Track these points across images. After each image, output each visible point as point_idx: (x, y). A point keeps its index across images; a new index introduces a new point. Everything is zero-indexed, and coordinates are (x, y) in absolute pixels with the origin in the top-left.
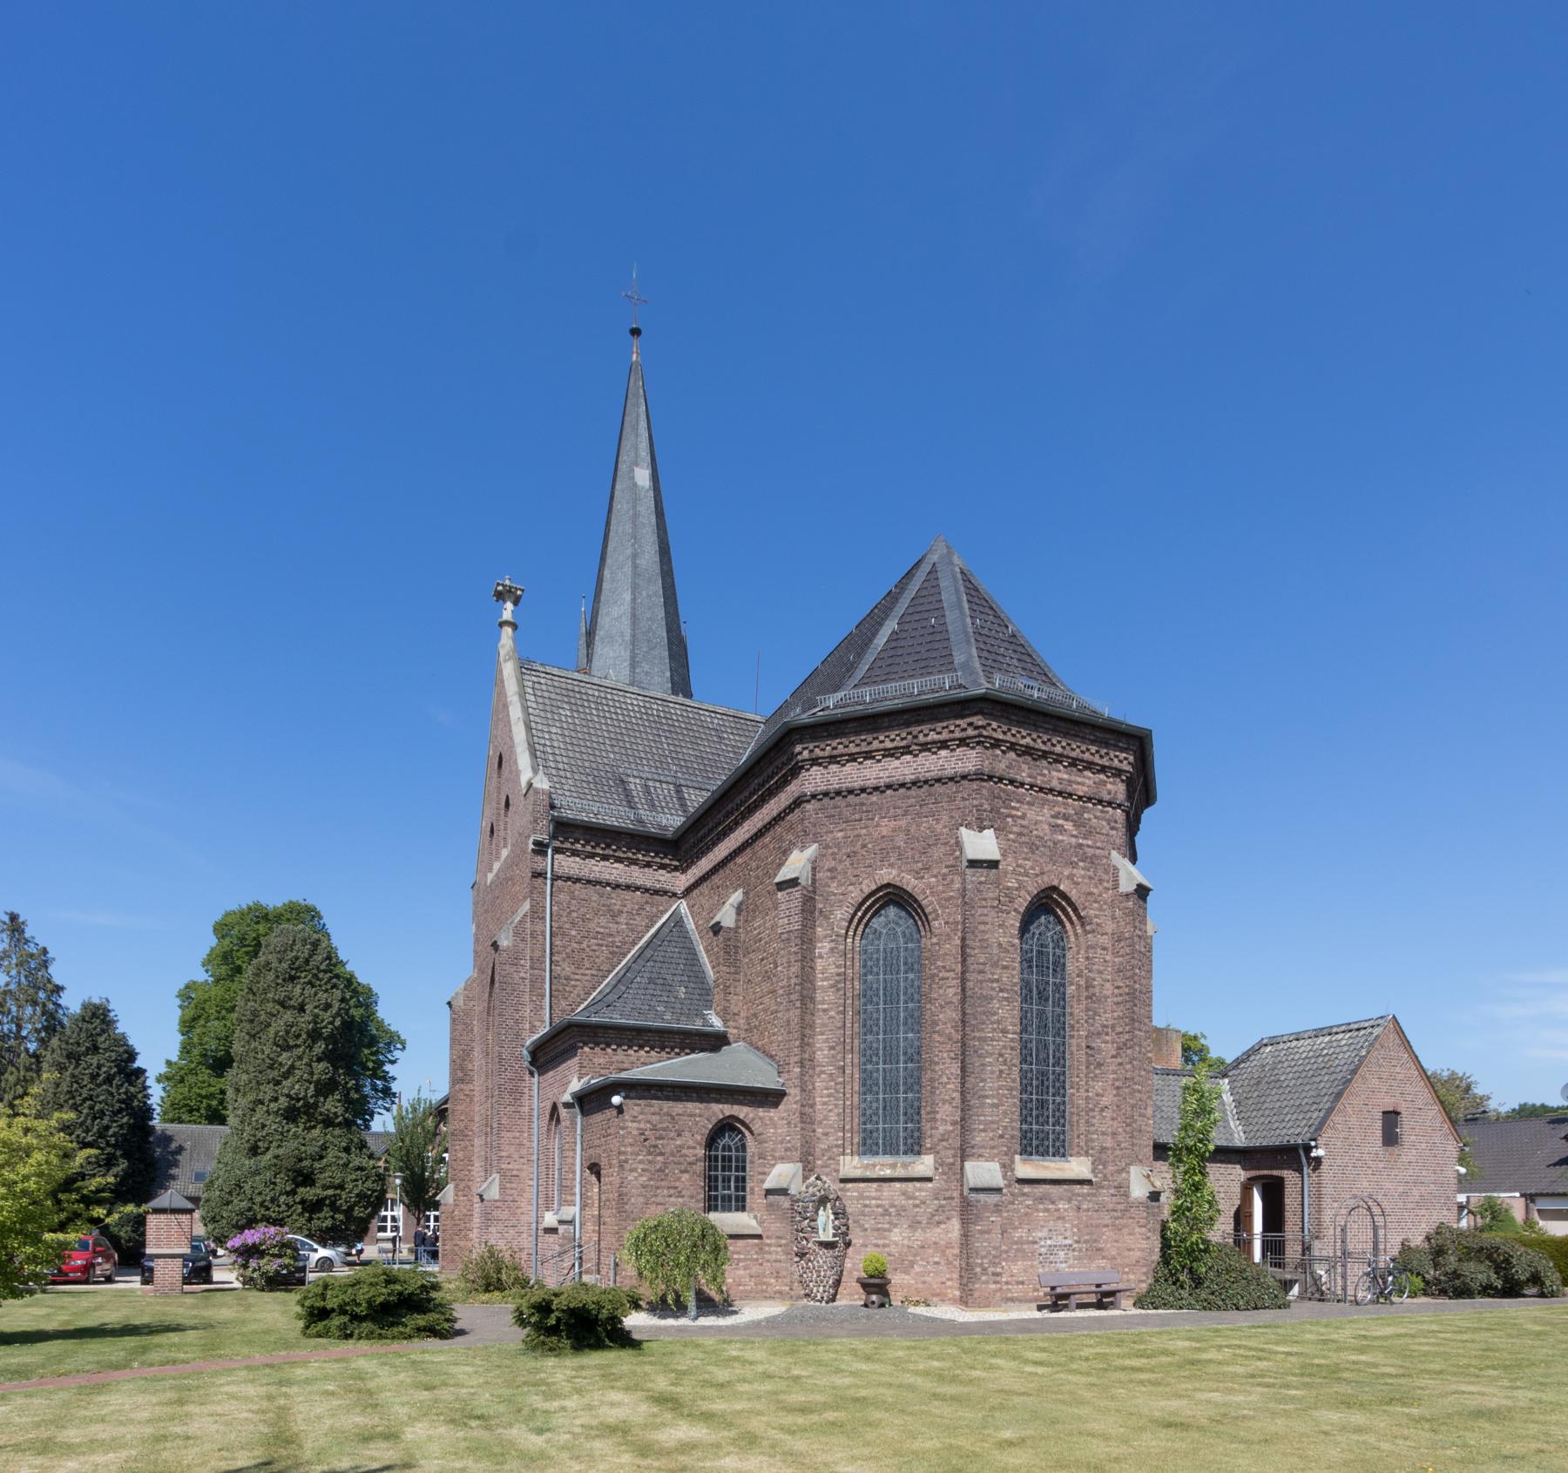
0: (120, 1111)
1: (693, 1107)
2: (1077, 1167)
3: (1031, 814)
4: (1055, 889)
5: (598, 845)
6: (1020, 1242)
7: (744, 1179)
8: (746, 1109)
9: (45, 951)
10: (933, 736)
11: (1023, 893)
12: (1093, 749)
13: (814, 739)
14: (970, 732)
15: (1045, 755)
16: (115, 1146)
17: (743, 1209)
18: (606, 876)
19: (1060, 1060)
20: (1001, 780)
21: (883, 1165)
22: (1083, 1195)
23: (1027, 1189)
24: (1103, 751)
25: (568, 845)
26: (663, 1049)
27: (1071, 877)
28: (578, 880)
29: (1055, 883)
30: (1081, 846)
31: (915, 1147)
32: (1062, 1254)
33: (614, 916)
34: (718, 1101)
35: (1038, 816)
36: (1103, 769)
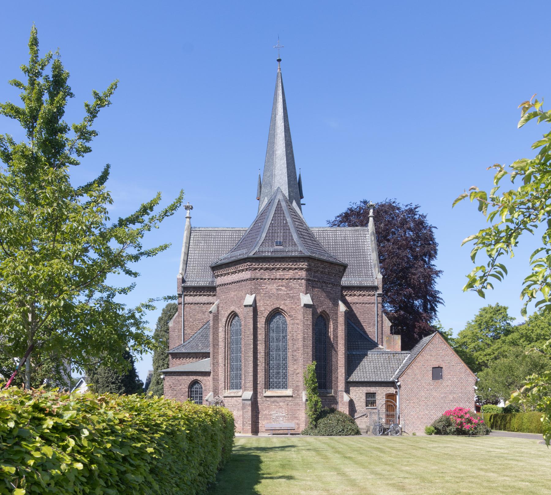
1: (184, 377)
2: (289, 392)
4: (279, 308)
5: (197, 292)
6: (266, 415)
7: (202, 397)
8: (200, 377)
10: (241, 268)
11: (266, 311)
12: (291, 264)
13: (217, 270)
14: (248, 267)
15: (273, 269)
16: (121, 383)
18: (201, 301)
19: (285, 359)
20: (258, 279)
21: (232, 392)
22: (289, 401)
23: (268, 399)
24: (295, 264)
25: (188, 293)
26: (197, 358)
27: (284, 304)
28: (192, 304)
29: (278, 306)
30: (288, 294)
31: (285, 387)
32: (281, 418)
33: (204, 313)
34: (192, 375)
35: (272, 287)
36: (296, 269)
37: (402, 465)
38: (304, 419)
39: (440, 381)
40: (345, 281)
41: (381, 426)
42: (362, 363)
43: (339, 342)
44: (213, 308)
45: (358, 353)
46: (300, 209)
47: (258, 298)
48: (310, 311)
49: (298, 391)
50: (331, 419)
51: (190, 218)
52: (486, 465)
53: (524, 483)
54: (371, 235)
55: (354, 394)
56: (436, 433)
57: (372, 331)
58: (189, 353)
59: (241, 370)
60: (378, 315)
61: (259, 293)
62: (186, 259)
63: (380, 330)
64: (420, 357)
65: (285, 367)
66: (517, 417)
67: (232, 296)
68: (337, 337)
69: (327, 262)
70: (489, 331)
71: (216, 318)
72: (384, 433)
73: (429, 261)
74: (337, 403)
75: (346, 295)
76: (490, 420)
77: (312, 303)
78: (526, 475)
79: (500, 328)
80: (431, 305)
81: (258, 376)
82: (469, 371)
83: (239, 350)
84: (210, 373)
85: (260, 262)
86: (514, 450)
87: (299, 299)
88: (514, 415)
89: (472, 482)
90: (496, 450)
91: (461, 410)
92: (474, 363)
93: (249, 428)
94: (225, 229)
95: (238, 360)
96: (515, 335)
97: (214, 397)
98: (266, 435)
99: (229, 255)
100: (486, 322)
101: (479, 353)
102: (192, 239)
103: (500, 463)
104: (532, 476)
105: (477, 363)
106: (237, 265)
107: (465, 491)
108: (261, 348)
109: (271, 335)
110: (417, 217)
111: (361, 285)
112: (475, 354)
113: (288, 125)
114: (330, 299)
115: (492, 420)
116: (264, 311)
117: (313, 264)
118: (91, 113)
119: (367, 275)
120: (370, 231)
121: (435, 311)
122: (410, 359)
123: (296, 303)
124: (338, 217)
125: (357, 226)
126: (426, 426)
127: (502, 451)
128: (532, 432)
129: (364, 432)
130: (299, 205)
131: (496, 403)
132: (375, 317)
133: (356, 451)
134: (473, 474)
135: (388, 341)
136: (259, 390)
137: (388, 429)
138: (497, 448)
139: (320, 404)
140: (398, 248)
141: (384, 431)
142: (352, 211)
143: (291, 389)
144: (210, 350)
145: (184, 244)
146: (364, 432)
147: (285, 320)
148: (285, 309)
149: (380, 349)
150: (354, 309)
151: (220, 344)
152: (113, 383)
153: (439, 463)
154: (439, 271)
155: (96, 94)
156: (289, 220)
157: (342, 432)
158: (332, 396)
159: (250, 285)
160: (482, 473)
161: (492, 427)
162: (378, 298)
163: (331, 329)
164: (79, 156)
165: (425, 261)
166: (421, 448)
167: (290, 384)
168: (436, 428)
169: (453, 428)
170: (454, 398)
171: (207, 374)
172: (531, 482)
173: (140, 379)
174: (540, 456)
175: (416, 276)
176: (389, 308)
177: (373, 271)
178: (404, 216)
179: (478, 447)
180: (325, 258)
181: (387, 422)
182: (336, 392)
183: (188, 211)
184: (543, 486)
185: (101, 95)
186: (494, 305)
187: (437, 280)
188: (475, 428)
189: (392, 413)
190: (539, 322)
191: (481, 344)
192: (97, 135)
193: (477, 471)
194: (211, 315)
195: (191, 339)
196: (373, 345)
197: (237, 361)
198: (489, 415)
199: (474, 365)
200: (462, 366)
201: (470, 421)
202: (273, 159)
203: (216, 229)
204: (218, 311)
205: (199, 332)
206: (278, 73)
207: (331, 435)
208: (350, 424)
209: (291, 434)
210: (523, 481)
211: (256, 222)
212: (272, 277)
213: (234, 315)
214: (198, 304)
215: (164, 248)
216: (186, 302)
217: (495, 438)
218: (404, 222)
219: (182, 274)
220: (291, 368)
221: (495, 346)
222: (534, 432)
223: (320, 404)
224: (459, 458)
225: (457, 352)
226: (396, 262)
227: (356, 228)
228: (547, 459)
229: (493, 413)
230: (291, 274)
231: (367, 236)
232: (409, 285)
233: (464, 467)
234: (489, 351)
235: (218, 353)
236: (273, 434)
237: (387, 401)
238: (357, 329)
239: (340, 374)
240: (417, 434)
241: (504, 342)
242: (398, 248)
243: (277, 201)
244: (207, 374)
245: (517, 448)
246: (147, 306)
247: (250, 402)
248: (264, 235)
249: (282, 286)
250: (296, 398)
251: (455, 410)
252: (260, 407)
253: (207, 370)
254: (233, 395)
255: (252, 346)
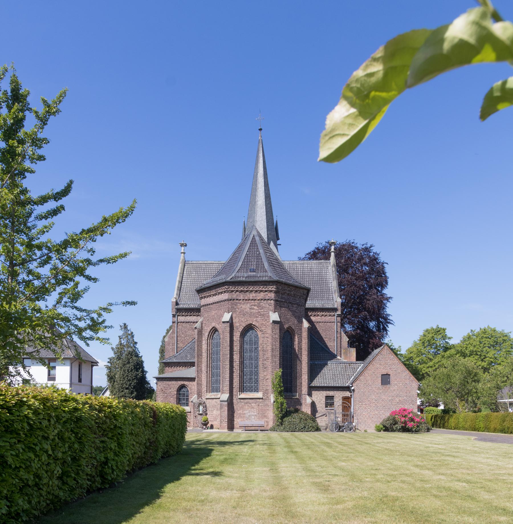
0: (135, 379)
1: (173, 382)
2: (259, 395)
3: (244, 306)
6: (240, 414)
9: (132, 333)
10: (220, 291)
11: (241, 326)
12: (262, 287)
15: (247, 291)
16: (133, 388)
17: (188, 406)
18: (191, 320)
19: (257, 367)
22: (260, 402)
23: (242, 401)
27: (256, 321)
28: (183, 322)
30: (259, 312)
31: (257, 390)
32: (253, 417)
35: (246, 307)
36: (266, 291)
37: (340, 460)
38: (272, 417)
39: (388, 386)
40: (309, 304)
41: (337, 424)
42: (323, 371)
43: (303, 353)
44: (198, 325)
45: (319, 363)
46: (277, 248)
47: (234, 316)
48: (277, 326)
49: (267, 394)
50: (294, 418)
51: (184, 253)
52: (422, 461)
53: (461, 484)
54: (332, 267)
55: (316, 397)
56: (385, 431)
57: (332, 345)
58: (179, 363)
59: (220, 376)
60: (337, 332)
61: (235, 312)
62: (180, 286)
63: (339, 344)
64: (371, 365)
65: (257, 374)
66: (454, 417)
67: (213, 314)
68: (301, 349)
69: (293, 286)
70: (431, 348)
71: (200, 333)
72: (339, 430)
73: (382, 290)
74: (301, 404)
75: (311, 315)
76: (431, 420)
77: (279, 320)
78: (463, 473)
79: (440, 345)
80: (383, 326)
81: (234, 381)
82: (413, 378)
83: (218, 360)
84: (195, 378)
85: (236, 286)
86: (450, 446)
87: (268, 317)
88: (452, 415)
89: (403, 482)
90: (436, 446)
91: (405, 410)
92: (419, 374)
93: (225, 425)
94: (213, 262)
95: (218, 367)
96: (453, 351)
97: (198, 398)
98: (240, 431)
99: (209, 281)
100: (428, 341)
101: (423, 365)
102: (185, 270)
103: (437, 459)
104: (468, 474)
105: (421, 373)
106: (217, 288)
107: (393, 494)
108: (236, 358)
109: (245, 346)
110: (371, 254)
111: (323, 307)
112: (420, 366)
113: (268, 181)
114: (295, 317)
115: (433, 420)
116: (239, 326)
117: (280, 287)
118: (42, 121)
119: (328, 299)
120: (332, 264)
121: (386, 330)
122: (363, 367)
123: (266, 320)
124: (307, 254)
125: (321, 260)
126: (376, 425)
127: (440, 447)
128: (466, 430)
129: (323, 429)
130: (276, 245)
131: (437, 406)
132: (334, 333)
133: (307, 445)
134: (408, 472)
135: (346, 353)
136: (234, 393)
137: (343, 426)
138: (436, 444)
139: (285, 405)
140: (356, 279)
141: (340, 428)
142: (319, 250)
143: (262, 393)
144: (195, 360)
145: (179, 275)
146: (323, 429)
147: (257, 334)
148: (257, 325)
149: (339, 359)
150: (318, 327)
151: (203, 354)
152: (127, 389)
153: (376, 458)
154: (389, 298)
155: (45, 101)
156: (261, 251)
157: (304, 429)
158: (297, 399)
159: (227, 305)
160: (417, 470)
161: (433, 426)
162: (338, 318)
163: (296, 342)
164: (32, 163)
165: (378, 290)
166: (366, 443)
167: (260, 388)
168: (384, 426)
169: (399, 426)
170: (400, 400)
171: (192, 379)
172: (468, 482)
173: (152, 386)
174: (475, 452)
175: (370, 303)
176: (348, 328)
177: (334, 296)
178: (361, 253)
179: (418, 443)
180: (291, 282)
181: (343, 421)
182: (300, 395)
183: (183, 248)
184: (482, 488)
185: (50, 102)
186: (435, 327)
187: (388, 304)
188: (418, 426)
189: (347, 413)
190: (471, 341)
191: (425, 359)
192: (49, 142)
193: (412, 468)
194: (196, 331)
195: (182, 351)
196: (333, 356)
197: (217, 369)
198: (430, 415)
199: (417, 374)
200: (407, 373)
201: (412, 420)
202: (255, 209)
203: (206, 262)
204: (202, 327)
205: (188, 345)
206: (259, 140)
207: (295, 431)
208: (311, 422)
209: (261, 430)
210: (459, 480)
211: (234, 253)
212: (246, 298)
213: (214, 330)
214: (188, 322)
215: (124, 256)
216: (179, 321)
217: (435, 434)
218: (361, 258)
219: (176, 298)
220: (261, 375)
221: (436, 360)
222: (469, 430)
223: (285, 405)
224: (398, 454)
225: (405, 365)
226: (354, 290)
227: (320, 261)
228: (483, 455)
229: (433, 414)
230: (261, 295)
231: (329, 269)
232: (365, 309)
233: (400, 463)
234: (431, 364)
235: (201, 362)
236: (246, 430)
237: (343, 403)
238: (320, 343)
239: (303, 380)
240: (368, 431)
241: (443, 357)
242: (356, 279)
243: (252, 236)
244: (192, 379)
245: (453, 444)
246: (104, 309)
247: (226, 403)
248: (240, 264)
249: (254, 306)
250: (265, 399)
251: (400, 410)
252: (235, 407)
253: (193, 376)
254: (213, 397)
255: (229, 356)
